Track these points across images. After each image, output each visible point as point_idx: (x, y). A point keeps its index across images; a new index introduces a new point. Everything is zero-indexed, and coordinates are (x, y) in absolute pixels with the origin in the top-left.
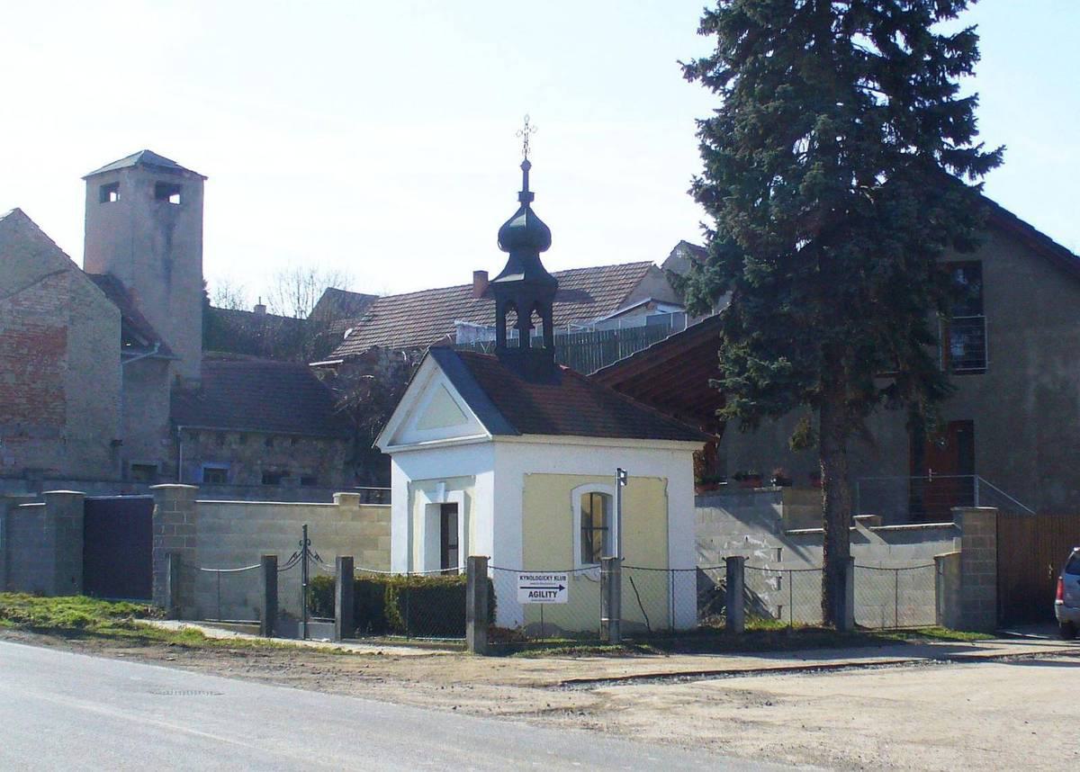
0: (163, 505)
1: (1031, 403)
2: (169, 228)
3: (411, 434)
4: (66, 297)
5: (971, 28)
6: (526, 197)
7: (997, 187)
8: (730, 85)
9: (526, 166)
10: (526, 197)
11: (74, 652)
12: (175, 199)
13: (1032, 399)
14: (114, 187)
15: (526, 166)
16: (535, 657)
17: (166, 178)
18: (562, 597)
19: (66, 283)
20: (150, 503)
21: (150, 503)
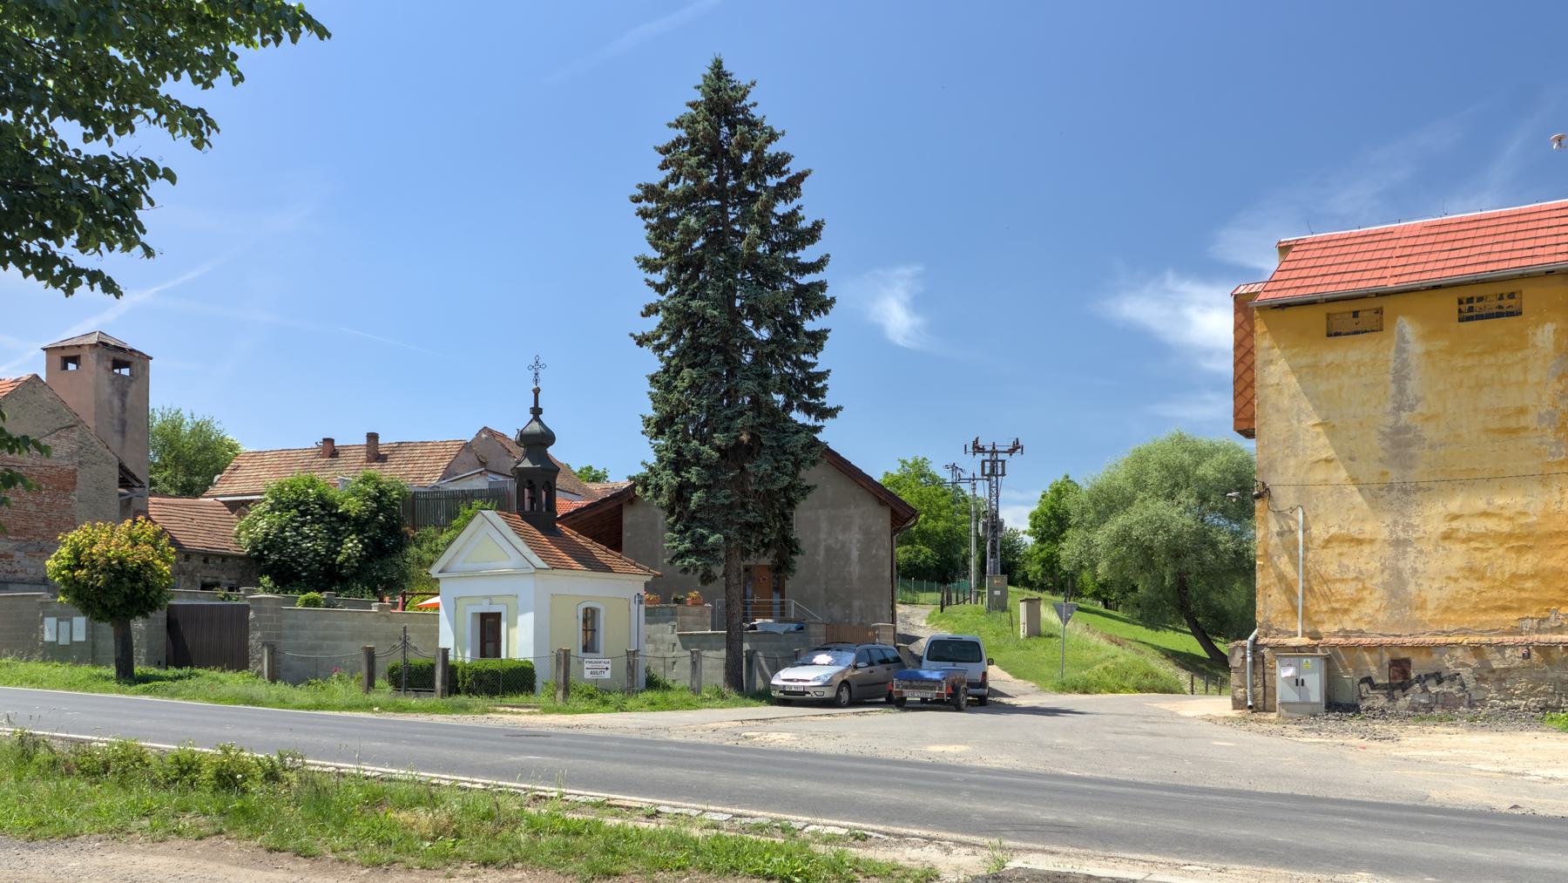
0: (258, 611)
1: (821, 557)
2: (123, 395)
3: (459, 565)
4: (75, 447)
5: (153, 170)
6: (536, 412)
7: (832, 434)
8: (667, 353)
9: (537, 392)
10: (536, 412)
11: (1319, 732)
12: (125, 372)
13: (822, 553)
14: (75, 360)
15: (537, 392)
16: (465, 709)
17: (120, 356)
18: (607, 675)
19: (75, 435)
20: (246, 609)
21: (246, 609)
